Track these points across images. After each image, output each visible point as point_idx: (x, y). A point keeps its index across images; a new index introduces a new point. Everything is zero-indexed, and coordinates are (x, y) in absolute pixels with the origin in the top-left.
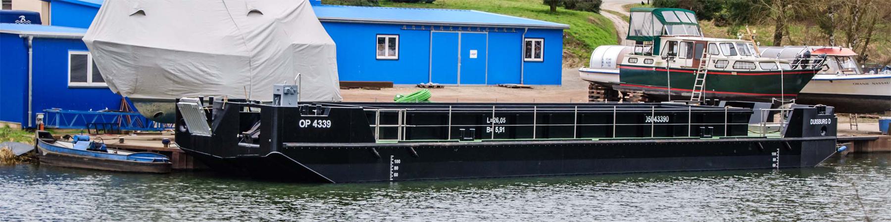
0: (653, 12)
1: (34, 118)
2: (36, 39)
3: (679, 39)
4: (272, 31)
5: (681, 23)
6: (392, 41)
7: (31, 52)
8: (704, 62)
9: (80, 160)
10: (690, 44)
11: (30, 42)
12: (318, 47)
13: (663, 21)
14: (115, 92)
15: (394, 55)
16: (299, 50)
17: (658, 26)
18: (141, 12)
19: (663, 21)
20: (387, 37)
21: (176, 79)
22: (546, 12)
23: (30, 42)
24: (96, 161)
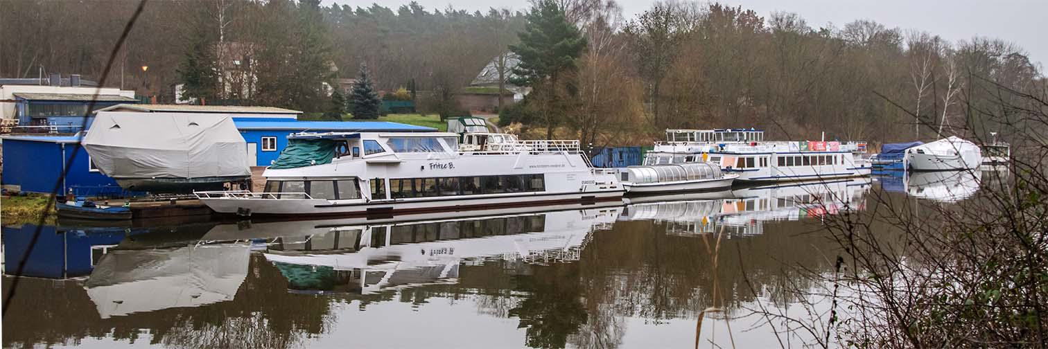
0: (459, 120)
1: (67, 191)
2: (66, 144)
3: (473, 134)
4: (203, 136)
5: (475, 125)
6: (272, 140)
7: (64, 153)
8: (486, 147)
9: (77, 213)
10: (478, 137)
11: (63, 146)
12: (233, 144)
13: (465, 125)
14: (103, 174)
15: (274, 148)
16: (221, 146)
17: (462, 127)
18: (117, 126)
19: (465, 125)
20: (269, 138)
21: (139, 165)
22: (438, 122)
23: (63, 146)
24: (86, 213)
